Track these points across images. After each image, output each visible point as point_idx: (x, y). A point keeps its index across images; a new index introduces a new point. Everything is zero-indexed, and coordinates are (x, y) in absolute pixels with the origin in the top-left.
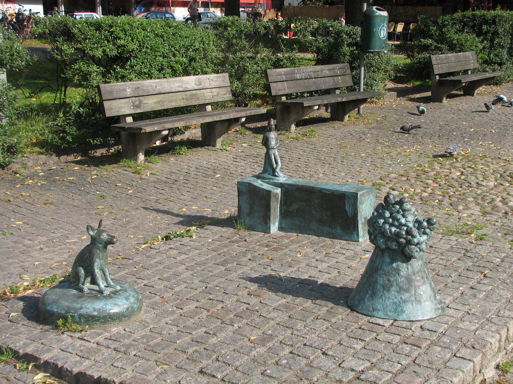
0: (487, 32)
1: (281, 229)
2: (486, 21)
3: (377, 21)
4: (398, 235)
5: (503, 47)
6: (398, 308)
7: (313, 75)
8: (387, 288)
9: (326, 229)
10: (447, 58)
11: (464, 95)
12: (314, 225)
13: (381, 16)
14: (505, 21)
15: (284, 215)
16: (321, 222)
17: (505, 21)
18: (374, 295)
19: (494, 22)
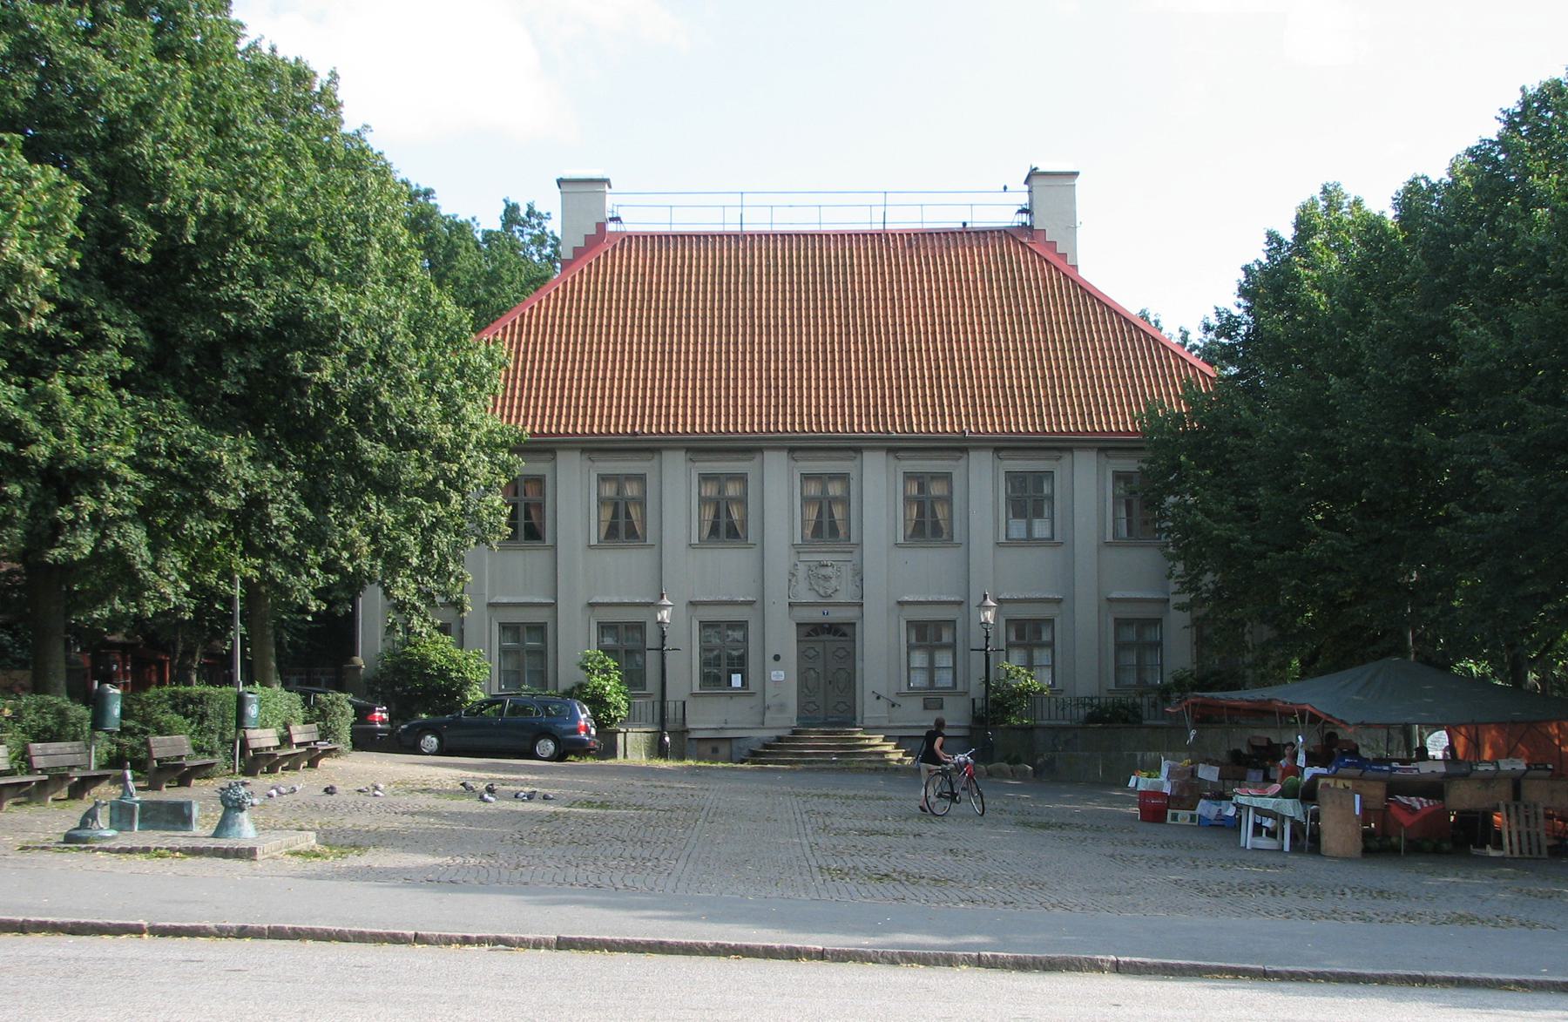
0: (194, 713)
1: (139, 829)
2: (191, 700)
3: (111, 698)
4: (238, 799)
5: (213, 732)
6: (239, 833)
7: (59, 751)
8: (233, 825)
9: (171, 826)
10: (163, 741)
11: (178, 786)
12: (163, 825)
13: (114, 694)
14: (214, 700)
15: (141, 821)
16: (167, 821)
17: (214, 700)
18: (227, 829)
19: (201, 702)
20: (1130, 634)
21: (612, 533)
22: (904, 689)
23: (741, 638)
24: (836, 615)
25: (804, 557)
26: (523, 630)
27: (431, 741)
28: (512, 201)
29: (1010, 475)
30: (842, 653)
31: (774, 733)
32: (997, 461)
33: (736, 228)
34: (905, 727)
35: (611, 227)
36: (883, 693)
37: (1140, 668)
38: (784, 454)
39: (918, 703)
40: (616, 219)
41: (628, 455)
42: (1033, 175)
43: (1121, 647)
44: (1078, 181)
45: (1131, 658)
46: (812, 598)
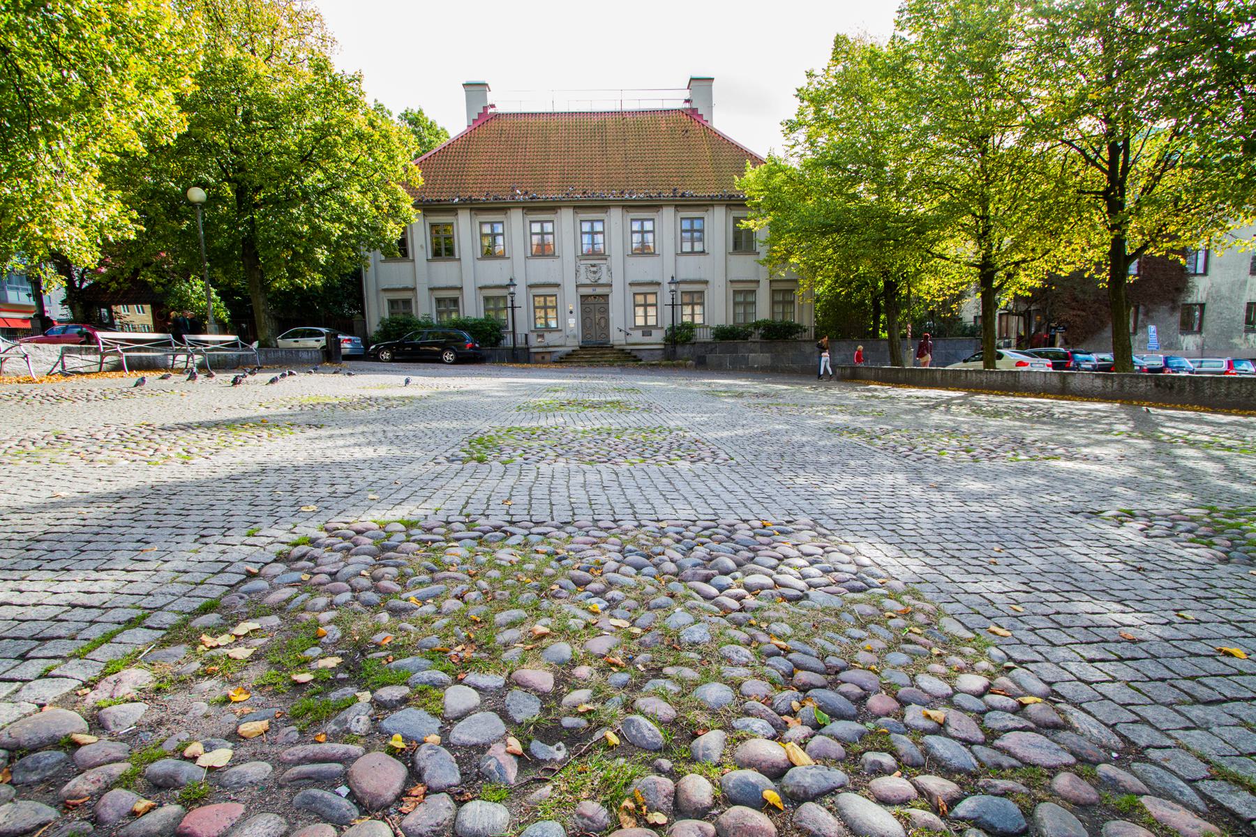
20: (740, 298)
21: (437, 254)
22: (533, 328)
23: (1198, 272)
24: (599, 291)
25: (583, 262)
26: (400, 303)
27: (386, 355)
28: (380, 102)
29: (433, 226)
30: (602, 310)
31: (570, 349)
32: (625, 214)
33: (618, 109)
34: (651, 344)
35: (490, 110)
36: (623, 328)
37: (745, 313)
38: (571, 211)
39: (640, 332)
40: (493, 106)
41: (598, 210)
42: (692, 79)
43: (736, 304)
44: (714, 83)
45: (741, 310)
46: (588, 282)
